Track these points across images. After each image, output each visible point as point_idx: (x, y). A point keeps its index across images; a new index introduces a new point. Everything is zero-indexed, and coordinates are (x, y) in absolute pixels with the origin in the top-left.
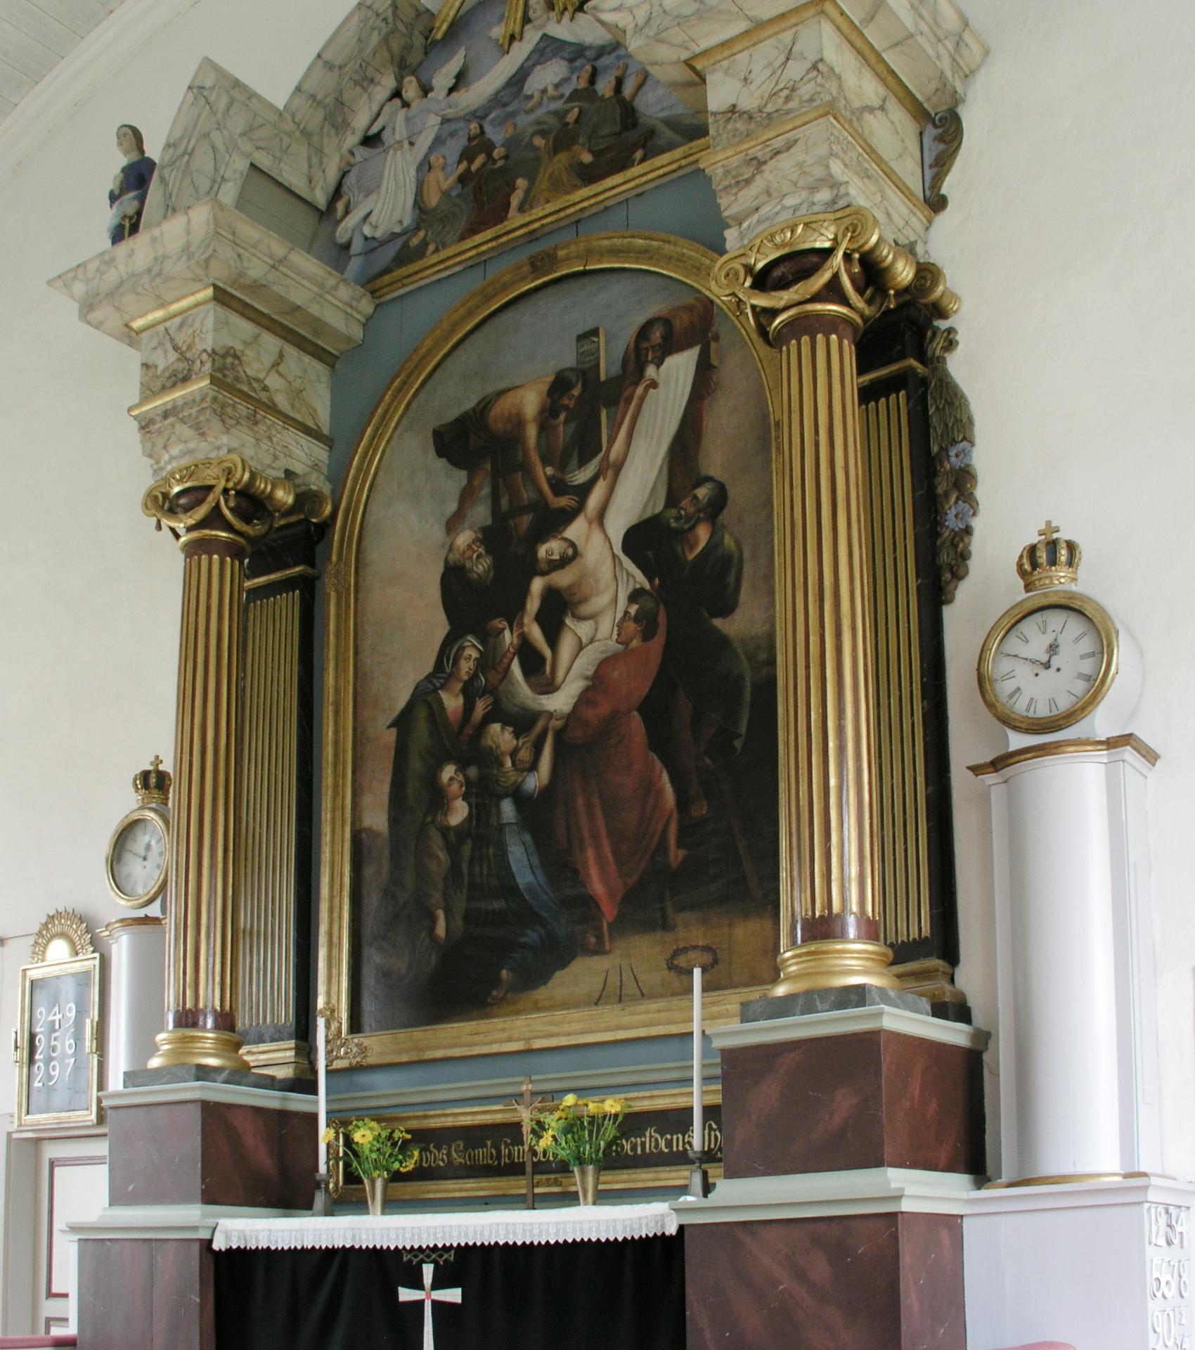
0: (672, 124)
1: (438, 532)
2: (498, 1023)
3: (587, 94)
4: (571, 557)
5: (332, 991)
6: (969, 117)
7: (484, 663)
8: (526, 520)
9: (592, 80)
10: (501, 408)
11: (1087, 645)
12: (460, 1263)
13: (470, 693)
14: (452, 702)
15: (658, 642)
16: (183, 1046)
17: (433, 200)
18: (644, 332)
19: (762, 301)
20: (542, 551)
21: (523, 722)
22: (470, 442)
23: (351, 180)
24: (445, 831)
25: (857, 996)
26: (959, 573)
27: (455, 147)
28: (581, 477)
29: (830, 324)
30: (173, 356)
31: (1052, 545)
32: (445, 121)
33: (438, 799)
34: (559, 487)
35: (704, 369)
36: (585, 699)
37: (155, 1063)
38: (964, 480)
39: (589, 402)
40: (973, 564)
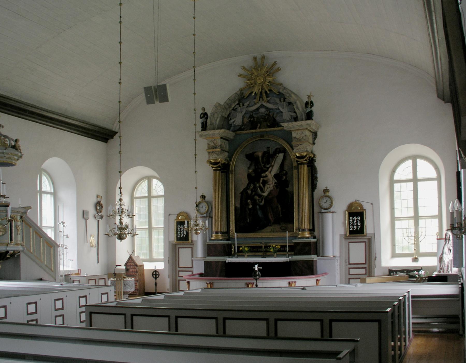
1: (247, 169)
2: (257, 234)
3: (268, 115)
4: (266, 176)
5: (233, 227)
6: (319, 134)
8: (260, 170)
9: (269, 113)
10: (256, 154)
11: (330, 201)
12: (260, 264)
13: (252, 191)
14: (249, 192)
15: (278, 190)
16: (217, 236)
17: (245, 122)
18: (277, 149)
19: (298, 160)
20: (262, 175)
21: (260, 196)
22: (251, 157)
23: (231, 115)
24: (249, 208)
25: (308, 238)
26: (315, 188)
27: (247, 116)
28: (268, 166)
29: (305, 164)
30: (213, 144)
31: (327, 190)
32: (246, 111)
33: (248, 204)
34: (265, 167)
36: (268, 195)
37: (213, 238)
38: (316, 178)
39: (269, 157)
40: (317, 187)
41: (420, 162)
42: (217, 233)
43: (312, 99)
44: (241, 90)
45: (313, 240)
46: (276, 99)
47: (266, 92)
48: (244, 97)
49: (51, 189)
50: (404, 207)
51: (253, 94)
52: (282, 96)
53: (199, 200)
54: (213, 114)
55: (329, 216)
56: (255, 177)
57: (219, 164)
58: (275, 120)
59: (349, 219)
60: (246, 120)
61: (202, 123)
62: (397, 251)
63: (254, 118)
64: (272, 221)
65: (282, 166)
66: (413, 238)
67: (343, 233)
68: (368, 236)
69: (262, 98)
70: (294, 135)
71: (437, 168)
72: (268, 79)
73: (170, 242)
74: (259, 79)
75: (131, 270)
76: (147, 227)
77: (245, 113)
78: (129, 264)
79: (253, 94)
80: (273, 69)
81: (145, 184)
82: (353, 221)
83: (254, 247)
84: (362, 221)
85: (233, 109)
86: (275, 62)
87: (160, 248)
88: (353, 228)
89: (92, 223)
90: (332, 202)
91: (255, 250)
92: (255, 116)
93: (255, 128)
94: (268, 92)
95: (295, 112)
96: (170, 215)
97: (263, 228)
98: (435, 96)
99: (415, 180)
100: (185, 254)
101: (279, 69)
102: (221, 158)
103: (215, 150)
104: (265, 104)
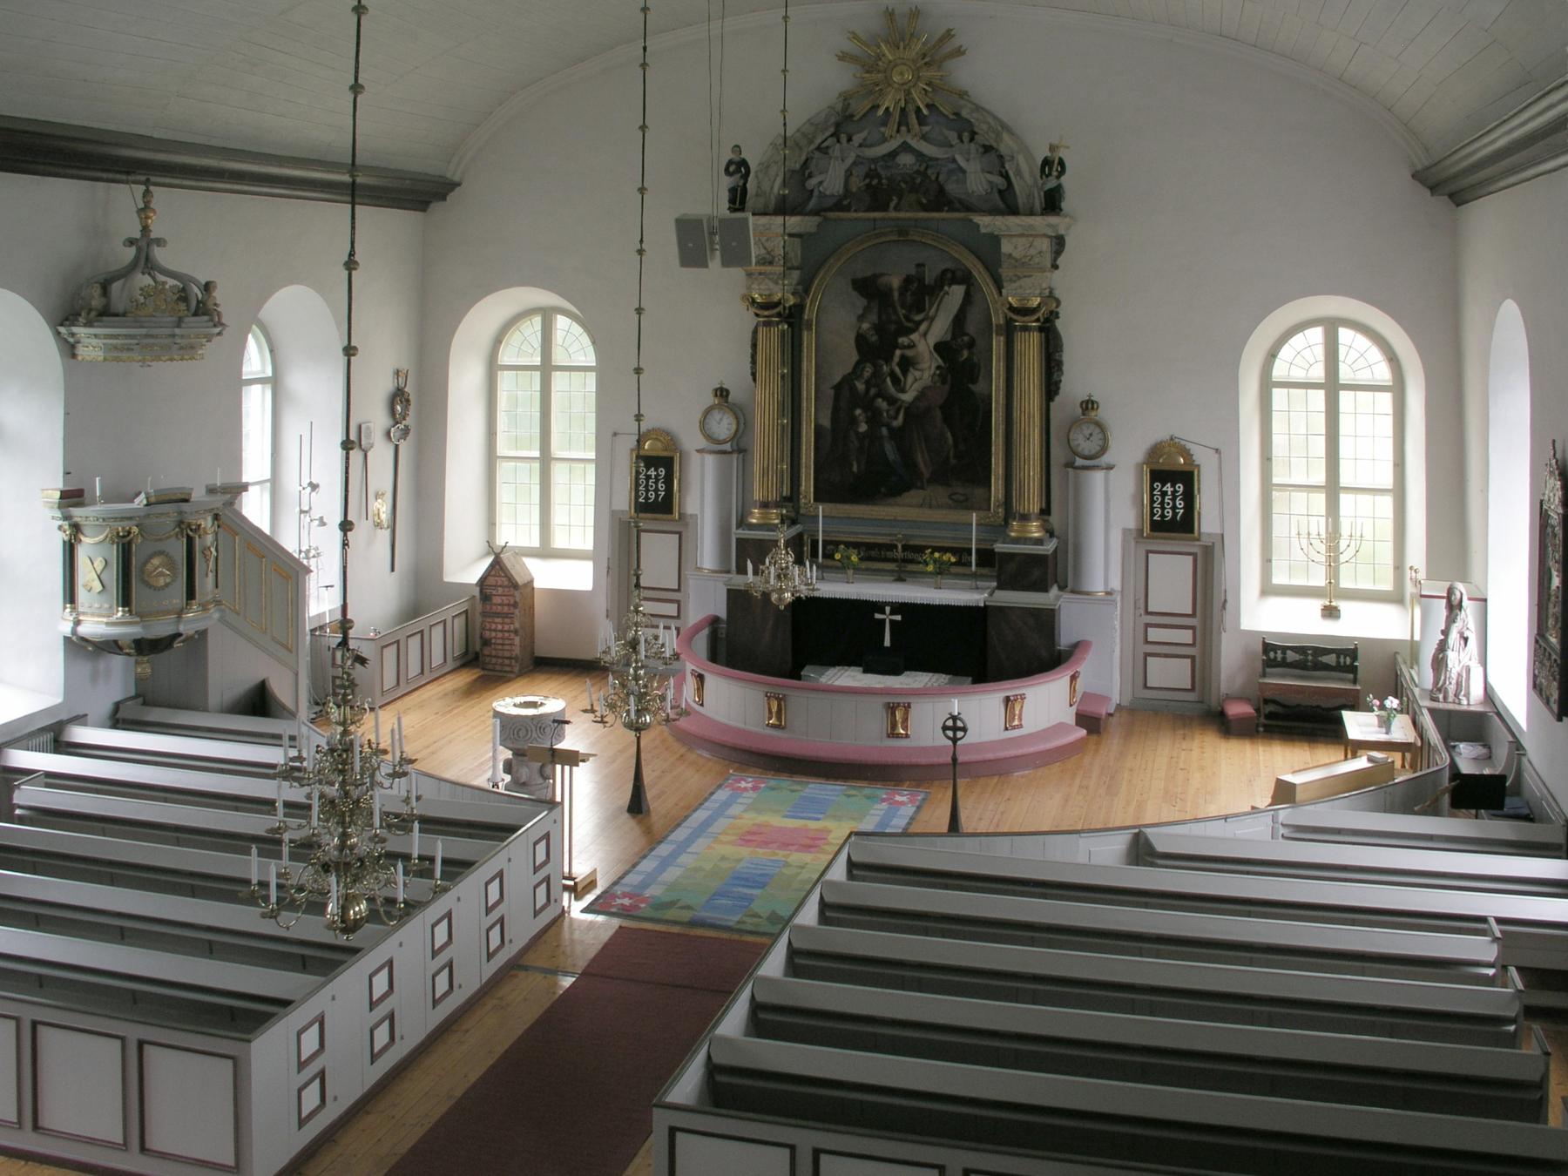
0: (960, 201)
4: (912, 346)
5: (807, 485)
7: (874, 375)
8: (893, 327)
10: (883, 280)
12: (898, 607)
13: (867, 383)
14: (860, 386)
15: (947, 387)
16: (764, 516)
18: (944, 272)
20: (900, 340)
21: (892, 401)
22: (868, 287)
24: (857, 433)
25: (1039, 542)
26: (1057, 392)
27: (861, 171)
28: (918, 318)
33: (854, 421)
34: (908, 319)
35: (967, 299)
36: (917, 399)
38: (1059, 364)
39: (921, 293)
41: (1345, 334)
42: (765, 505)
43: (1062, 153)
44: (846, 97)
45: (1049, 547)
46: (947, 132)
47: (918, 110)
48: (852, 116)
49: (263, 364)
50: (1298, 457)
51: (881, 112)
52: (966, 129)
53: (710, 400)
54: (765, 167)
55: (1098, 477)
56: (879, 347)
57: (780, 309)
58: (941, 190)
59: (1152, 489)
60: (857, 183)
61: (733, 191)
62: (1278, 579)
63: (878, 176)
64: (927, 475)
65: (959, 321)
66: (1322, 548)
67: (1131, 523)
68: (1205, 541)
69: (907, 125)
70: (1006, 247)
71: (1393, 359)
72: (926, 74)
73: (613, 513)
74: (902, 74)
75: (497, 600)
76: (537, 454)
77: (854, 163)
78: (491, 580)
79: (881, 112)
80: (942, 50)
81: (534, 326)
82: (1164, 494)
83: (880, 546)
84: (1189, 497)
85: (818, 148)
86: (949, 31)
87: (578, 517)
88: (1163, 516)
89: (381, 455)
90: (1105, 439)
91: (873, 553)
92: (883, 173)
93: (885, 208)
94: (925, 112)
95: (1006, 176)
96: (615, 434)
97: (900, 494)
98: (1407, 174)
99: (1332, 386)
100: (658, 553)
101: (959, 52)
102: (782, 291)
103: (768, 269)
104: (914, 143)
